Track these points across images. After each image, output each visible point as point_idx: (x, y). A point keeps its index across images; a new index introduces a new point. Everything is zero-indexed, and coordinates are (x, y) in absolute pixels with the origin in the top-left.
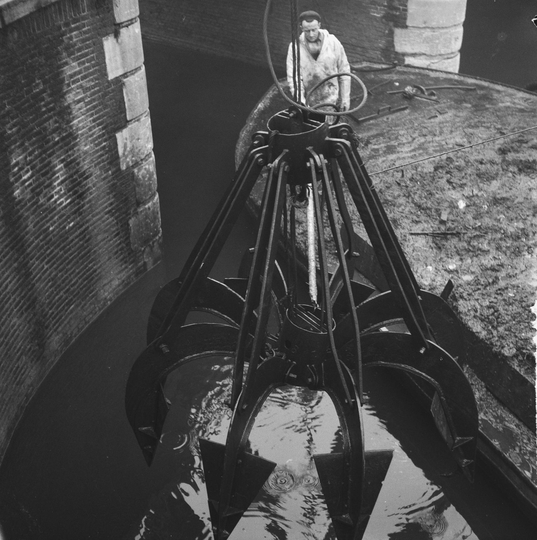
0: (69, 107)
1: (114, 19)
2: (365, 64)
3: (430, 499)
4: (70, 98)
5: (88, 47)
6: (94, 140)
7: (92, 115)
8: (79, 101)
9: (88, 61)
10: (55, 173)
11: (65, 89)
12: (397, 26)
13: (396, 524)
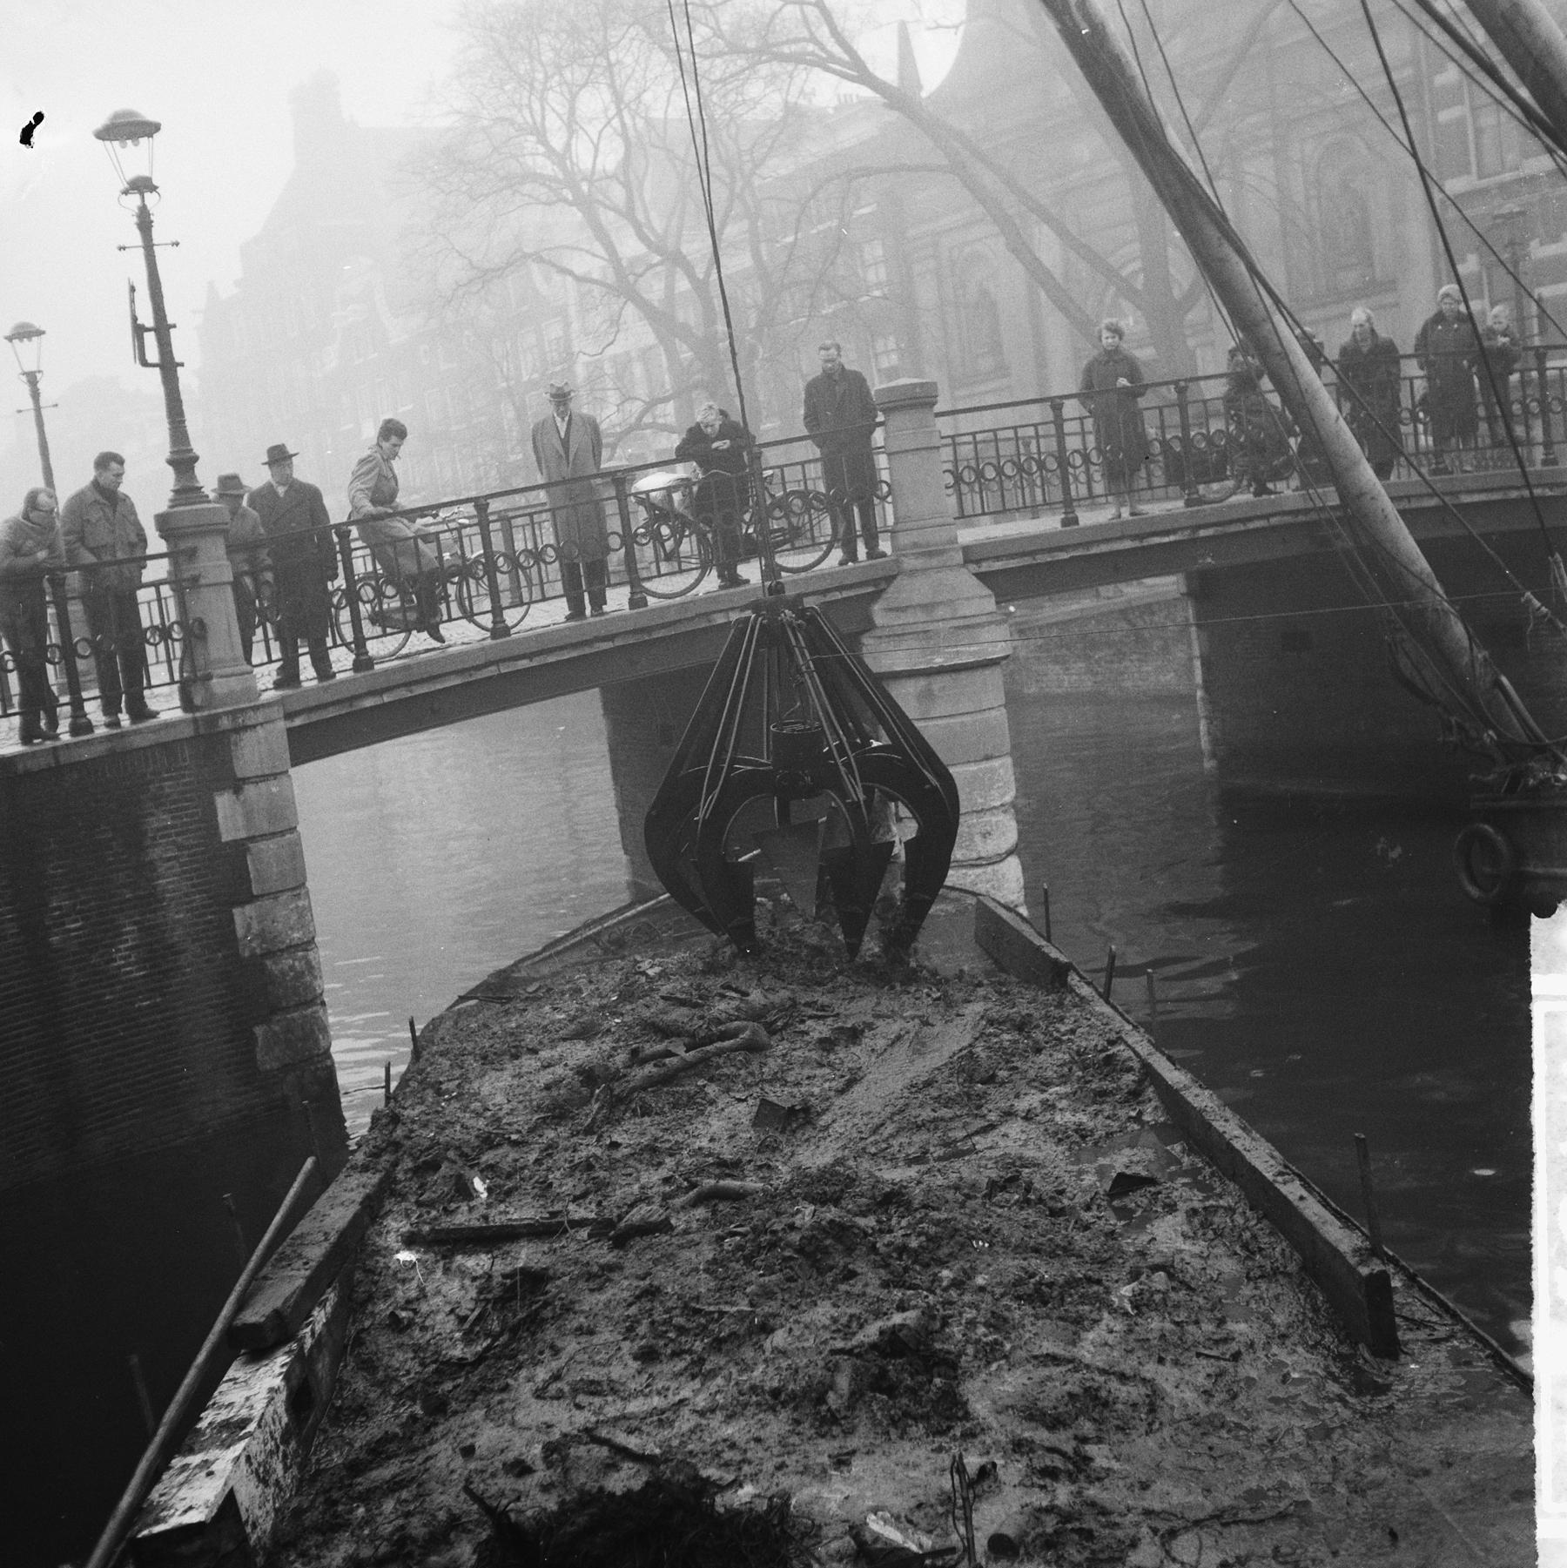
1: (232, 769)
4: (155, 853)
5: (191, 800)
6: (192, 910)
8: (169, 859)
10: (123, 934)
11: (148, 842)
13: (101, 121)
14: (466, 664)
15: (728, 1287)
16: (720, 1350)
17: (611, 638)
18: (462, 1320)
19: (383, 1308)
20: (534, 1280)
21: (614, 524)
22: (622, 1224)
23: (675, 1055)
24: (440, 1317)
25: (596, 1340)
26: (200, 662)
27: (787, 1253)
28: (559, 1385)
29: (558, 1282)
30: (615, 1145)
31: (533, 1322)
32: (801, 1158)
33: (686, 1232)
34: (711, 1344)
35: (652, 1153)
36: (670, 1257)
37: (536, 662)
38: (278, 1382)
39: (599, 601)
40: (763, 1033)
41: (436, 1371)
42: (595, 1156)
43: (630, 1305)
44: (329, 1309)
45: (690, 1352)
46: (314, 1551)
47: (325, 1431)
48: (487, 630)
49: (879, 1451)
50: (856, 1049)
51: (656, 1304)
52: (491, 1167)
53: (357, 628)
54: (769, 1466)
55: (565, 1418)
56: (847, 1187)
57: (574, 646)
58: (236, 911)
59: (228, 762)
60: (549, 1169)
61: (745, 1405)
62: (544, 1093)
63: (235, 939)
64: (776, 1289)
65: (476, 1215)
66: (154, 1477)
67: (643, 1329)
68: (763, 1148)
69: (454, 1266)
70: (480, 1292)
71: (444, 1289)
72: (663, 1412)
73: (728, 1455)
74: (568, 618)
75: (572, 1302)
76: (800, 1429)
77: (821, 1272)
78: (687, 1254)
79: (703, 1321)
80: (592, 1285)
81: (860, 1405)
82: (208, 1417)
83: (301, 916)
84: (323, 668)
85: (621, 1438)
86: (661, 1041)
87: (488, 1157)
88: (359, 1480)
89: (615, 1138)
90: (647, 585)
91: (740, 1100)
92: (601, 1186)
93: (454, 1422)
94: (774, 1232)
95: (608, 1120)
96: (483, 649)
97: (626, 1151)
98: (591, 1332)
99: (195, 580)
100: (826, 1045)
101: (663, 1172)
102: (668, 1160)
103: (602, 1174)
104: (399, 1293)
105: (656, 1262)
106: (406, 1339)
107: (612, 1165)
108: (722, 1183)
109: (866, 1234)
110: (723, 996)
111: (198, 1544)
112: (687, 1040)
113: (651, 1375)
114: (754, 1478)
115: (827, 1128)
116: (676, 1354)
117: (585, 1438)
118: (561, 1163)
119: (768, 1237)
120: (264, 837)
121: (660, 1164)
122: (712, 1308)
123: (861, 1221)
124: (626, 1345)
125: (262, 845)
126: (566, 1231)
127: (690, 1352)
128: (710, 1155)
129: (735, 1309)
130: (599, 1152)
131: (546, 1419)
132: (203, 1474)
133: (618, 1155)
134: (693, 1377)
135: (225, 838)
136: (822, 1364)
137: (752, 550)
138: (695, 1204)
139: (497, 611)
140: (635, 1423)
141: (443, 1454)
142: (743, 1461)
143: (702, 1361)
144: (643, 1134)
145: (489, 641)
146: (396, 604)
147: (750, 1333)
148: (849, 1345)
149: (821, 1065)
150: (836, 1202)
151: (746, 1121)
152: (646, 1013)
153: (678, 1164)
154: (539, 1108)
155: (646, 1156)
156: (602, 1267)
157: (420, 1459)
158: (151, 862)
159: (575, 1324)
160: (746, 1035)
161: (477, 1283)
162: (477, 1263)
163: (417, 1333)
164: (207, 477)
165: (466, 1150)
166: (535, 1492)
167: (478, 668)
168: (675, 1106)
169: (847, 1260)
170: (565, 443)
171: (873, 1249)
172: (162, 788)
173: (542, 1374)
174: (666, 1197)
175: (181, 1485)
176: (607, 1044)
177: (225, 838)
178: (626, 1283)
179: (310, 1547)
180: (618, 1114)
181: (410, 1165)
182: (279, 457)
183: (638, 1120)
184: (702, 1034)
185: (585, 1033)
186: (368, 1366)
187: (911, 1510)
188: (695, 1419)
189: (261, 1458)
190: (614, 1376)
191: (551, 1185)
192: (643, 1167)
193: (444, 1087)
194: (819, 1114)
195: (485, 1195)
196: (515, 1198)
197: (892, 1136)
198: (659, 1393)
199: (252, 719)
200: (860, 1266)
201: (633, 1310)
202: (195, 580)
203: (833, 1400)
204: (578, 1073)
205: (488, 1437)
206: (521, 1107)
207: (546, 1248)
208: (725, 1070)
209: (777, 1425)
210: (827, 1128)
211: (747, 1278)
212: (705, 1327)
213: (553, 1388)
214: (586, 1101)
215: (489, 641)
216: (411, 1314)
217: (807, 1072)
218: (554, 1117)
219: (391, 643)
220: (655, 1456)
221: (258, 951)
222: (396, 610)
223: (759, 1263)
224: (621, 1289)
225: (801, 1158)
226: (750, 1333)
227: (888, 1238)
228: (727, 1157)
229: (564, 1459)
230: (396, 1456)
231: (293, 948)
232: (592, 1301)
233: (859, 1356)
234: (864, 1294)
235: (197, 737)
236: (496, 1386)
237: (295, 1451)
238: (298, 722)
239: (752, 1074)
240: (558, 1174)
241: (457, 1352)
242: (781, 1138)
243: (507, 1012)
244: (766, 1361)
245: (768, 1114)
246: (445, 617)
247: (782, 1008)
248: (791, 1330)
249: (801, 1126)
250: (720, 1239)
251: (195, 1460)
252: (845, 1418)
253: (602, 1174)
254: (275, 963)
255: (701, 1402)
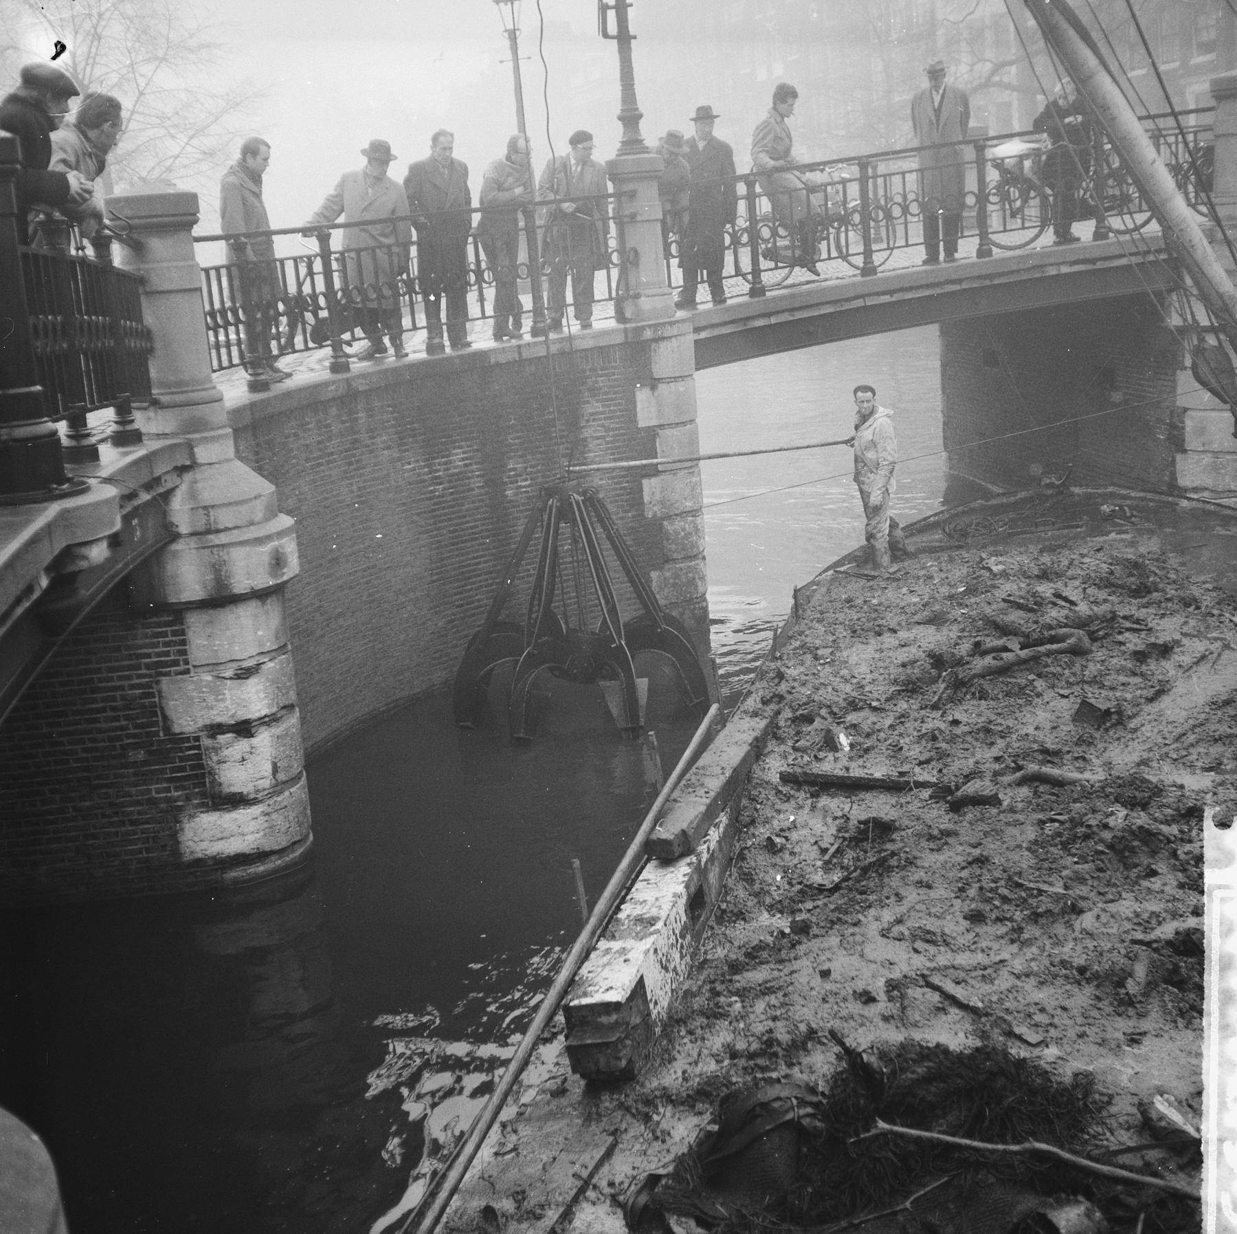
0: (585, 439)
2: (1110, 489)
3: (1219, 1209)
4: (587, 433)
6: (613, 478)
7: (613, 454)
8: (598, 438)
9: (615, 405)
11: (583, 423)
12: (1177, 451)
14: (837, 297)
15: (1047, 867)
16: (1036, 922)
17: (960, 281)
18: (824, 851)
19: (763, 832)
20: (883, 829)
21: (971, 183)
22: (959, 794)
23: (1010, 651)
24: (806, 846)
25: (933, 894)
26: (632, 282)
27: (1100, 848)
28: (901, 928)
29: (903, 833)
30: (956, 722)
31: (880, 866)
32: (1112, 754)
33: (1012, 810)
34: (1029, 917)
35: (986, 733)
36: (999, 832)
37: (896, 298)
38: (681, 889)
39: (951, 249)
40: (1086, 640)
41: (800, 891)
42: (938, 729)
43: (963, 868)
44: (721, 829)
45: (1011, 919)
46: (699, 1031)
47: (712, 928)
48: (857, 268)
49: (1166, 1036)
50: (1163, 663)
51: (985, 871)
52: (854, 726)
53: (755, 262)
54: (1072, 1033)
55: (906, 961)
56: (1154, 794)
57: (927, 286)
58: (645, 482)
59: (647, 365)
60: (901, 735)
61: (1055, 976)
62: (901, 669)
63: (643, 503)
64: (1087, 877)
65: (839, 765)
66: (585, 956)
67: (972, 892)
68: (1080, 741)
69: (820, 805)
70: (839, 831)
71: (811, 823)
72: (985, 968)
73: (1039, 1018)
74: (925, 263)
75: (915, 858)
76: (1100, 1005)
77: (1128, 867)
78: (1011, 831)
79: (1024, 894)
80: (932, 846)
81: (1154, 994)
82: (627, 910)
83: (693, 489)
84: (718, 294)
85: (950, 988)
86: (1000, 638)
87: (852, 718)
88: (737, 977)
89: (958, 716)
90: (993, 237)
91: (1063, 696)
92: (942, 755)
93: (815, 944)
94: (1089, 826)
95: (951, 700)
96: (854, 284)
97: (966, 729)
98: (929, 887)
99: (633, 217)
100: (1140, 656)
101: (995, 752)
102: (999, 741)
103: (944, 745)
104: (775, 822)
105: (986, 834)
106: (777, 860)
107: (952, 739)
108: (1044, 769)
109: (1169, 841)
110: (1055, 604)
111: (614, 1017)
112: (1021, 639)
113: (977, 935)
114: (1058, 1041)
115: (1135, 730)
116: (999, 920)
117: (922, 983)
118: (911, 731)
119: (1083, 829)
120: (670, 425)
121: (992, 744)
122: (1032, 885)
123: (1164, 829)
124: (957, 903)
125: (668, 432)
126: (911, 789)
127: (1011, 919)
128: (1035, 741)
129: (1051, 889)
130: (943, 726)
131: (889, 957)
132: (622, 959)
133: (958, 730)
134: (1013, 941)
135: (641, 424)
136: (1123, 951)
137: (1086, 212)
138: (1020, 783)
139: (868, 253)
140: (962, 975)
141: (804, 971)
142: (1051, 1024)
143: (1020, 930)
144: (979, 715)
145: (859, 278)
146: (786, 243)
147: (1063, 912)
148: (1148, 938)
149: (1134, 674)
150: (1144, 806)
151: (1067, 716)
152: (988, 611)
153: (1008, 746)
154: (896, 682)
155: (982, 735)
156: (941, 832)
157: (786, 971)
158: (585, 439)
159: (916, 877)
160: (1071, 641)
161: (838, 822)
162: (834, 804)
163: (787, 856)
164: (652, 133)
165: (835, 710)
166: (877, 1020)
167: (847, 300)
168: (1008, 694)
169: (1150, 860)
170: (938, 112)
171: (1174, 854)
172: (597, 382)
173: (888, 916)
174: (996, 774)
175: (604, 966)
176: (952, 632)
177: (641, 424)
178: (961, 848)
179: (696, 1028)
180: (960, 695)
181: (790, 715)
182: (705, 116)
183: (975, 702)
184: (1035, 636)
185: (936, 620)
186: (748, 878)
187: (1191, 1094)
188: (1012, 981)
189: (664, 951)
190: (947, 931)
191: (901, 748)
192: (978, 744)
193: (820, 652)
194: (1130, 717)
195: (847, 749)
196: (872, 755)
197: (1192, 745)
198: (983, 951)
199: (669, 331)
200: (1161, 867)
201: (965, 874)
202: (633, 217)
203: (1132, 987)
204: (929, 656)
205: (841, 963)
206: (881, 678)
207: (894, 802)
208: (1052, 669)
209: (1082, 997)
210: (1135, 730)
211: (1062, 862)
212: (1025, 900)
213: (896, 930)
214: (934, 681)
215: (859, 278)
216: (784, 841)
217: (1122, 679)
218: (907, 691)
219: (780, 274)
220: (977, 1008)
221: (659, 514)
222: (786, 248)
223: (1074, 851)
224: (955, 854)
225: (1112, 754)
226: (1063, 912)
227: (1188, 847)
228: (1050, 746)
229: (903, 997)
230: (768, 962)
231: (684, 514)
232: (930, 859)
233: (1156, 950)
234: (1162, 892)
235: (625, 344)
236: (848, 918)
237: (690, 944)
238: (703, 335)
239: (1074, 674)
240: (907, 740)
241: (818, 878)
242: (1097, 735)
243: (871, 588)
244: (1075, 939)
245: (1087, 713)
246: (824, 255)
247: (1104, 619)
248: (1098, 917)
249: (1114, 726)
250: (1041, 823)
251: (616, 945)
252: (1140, 1002)
253: (944, 745)
254: (672, 524)
255: (1018, 965)
